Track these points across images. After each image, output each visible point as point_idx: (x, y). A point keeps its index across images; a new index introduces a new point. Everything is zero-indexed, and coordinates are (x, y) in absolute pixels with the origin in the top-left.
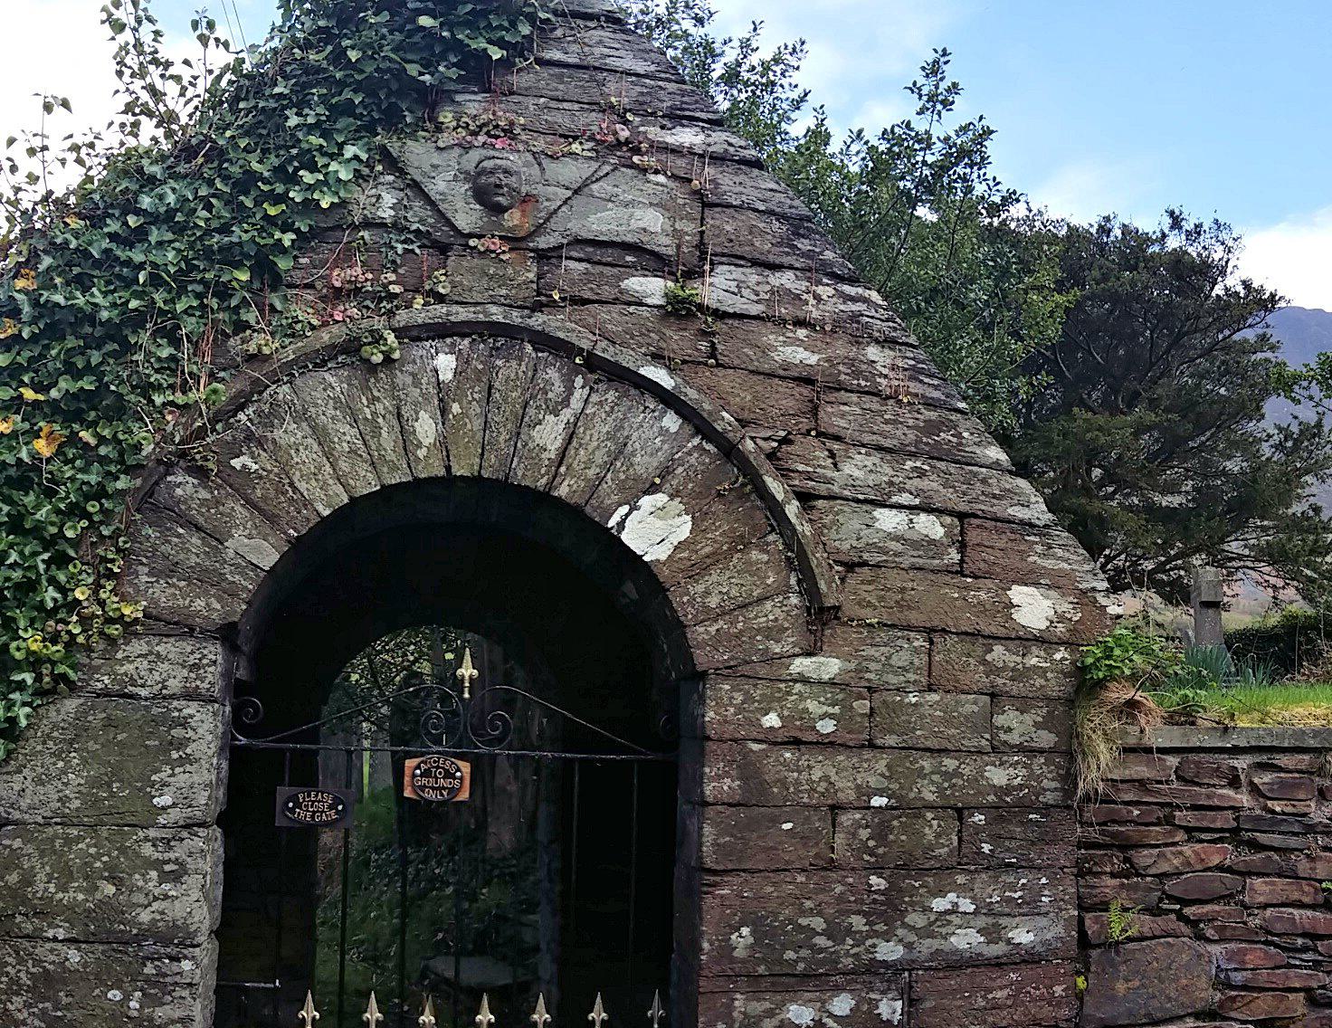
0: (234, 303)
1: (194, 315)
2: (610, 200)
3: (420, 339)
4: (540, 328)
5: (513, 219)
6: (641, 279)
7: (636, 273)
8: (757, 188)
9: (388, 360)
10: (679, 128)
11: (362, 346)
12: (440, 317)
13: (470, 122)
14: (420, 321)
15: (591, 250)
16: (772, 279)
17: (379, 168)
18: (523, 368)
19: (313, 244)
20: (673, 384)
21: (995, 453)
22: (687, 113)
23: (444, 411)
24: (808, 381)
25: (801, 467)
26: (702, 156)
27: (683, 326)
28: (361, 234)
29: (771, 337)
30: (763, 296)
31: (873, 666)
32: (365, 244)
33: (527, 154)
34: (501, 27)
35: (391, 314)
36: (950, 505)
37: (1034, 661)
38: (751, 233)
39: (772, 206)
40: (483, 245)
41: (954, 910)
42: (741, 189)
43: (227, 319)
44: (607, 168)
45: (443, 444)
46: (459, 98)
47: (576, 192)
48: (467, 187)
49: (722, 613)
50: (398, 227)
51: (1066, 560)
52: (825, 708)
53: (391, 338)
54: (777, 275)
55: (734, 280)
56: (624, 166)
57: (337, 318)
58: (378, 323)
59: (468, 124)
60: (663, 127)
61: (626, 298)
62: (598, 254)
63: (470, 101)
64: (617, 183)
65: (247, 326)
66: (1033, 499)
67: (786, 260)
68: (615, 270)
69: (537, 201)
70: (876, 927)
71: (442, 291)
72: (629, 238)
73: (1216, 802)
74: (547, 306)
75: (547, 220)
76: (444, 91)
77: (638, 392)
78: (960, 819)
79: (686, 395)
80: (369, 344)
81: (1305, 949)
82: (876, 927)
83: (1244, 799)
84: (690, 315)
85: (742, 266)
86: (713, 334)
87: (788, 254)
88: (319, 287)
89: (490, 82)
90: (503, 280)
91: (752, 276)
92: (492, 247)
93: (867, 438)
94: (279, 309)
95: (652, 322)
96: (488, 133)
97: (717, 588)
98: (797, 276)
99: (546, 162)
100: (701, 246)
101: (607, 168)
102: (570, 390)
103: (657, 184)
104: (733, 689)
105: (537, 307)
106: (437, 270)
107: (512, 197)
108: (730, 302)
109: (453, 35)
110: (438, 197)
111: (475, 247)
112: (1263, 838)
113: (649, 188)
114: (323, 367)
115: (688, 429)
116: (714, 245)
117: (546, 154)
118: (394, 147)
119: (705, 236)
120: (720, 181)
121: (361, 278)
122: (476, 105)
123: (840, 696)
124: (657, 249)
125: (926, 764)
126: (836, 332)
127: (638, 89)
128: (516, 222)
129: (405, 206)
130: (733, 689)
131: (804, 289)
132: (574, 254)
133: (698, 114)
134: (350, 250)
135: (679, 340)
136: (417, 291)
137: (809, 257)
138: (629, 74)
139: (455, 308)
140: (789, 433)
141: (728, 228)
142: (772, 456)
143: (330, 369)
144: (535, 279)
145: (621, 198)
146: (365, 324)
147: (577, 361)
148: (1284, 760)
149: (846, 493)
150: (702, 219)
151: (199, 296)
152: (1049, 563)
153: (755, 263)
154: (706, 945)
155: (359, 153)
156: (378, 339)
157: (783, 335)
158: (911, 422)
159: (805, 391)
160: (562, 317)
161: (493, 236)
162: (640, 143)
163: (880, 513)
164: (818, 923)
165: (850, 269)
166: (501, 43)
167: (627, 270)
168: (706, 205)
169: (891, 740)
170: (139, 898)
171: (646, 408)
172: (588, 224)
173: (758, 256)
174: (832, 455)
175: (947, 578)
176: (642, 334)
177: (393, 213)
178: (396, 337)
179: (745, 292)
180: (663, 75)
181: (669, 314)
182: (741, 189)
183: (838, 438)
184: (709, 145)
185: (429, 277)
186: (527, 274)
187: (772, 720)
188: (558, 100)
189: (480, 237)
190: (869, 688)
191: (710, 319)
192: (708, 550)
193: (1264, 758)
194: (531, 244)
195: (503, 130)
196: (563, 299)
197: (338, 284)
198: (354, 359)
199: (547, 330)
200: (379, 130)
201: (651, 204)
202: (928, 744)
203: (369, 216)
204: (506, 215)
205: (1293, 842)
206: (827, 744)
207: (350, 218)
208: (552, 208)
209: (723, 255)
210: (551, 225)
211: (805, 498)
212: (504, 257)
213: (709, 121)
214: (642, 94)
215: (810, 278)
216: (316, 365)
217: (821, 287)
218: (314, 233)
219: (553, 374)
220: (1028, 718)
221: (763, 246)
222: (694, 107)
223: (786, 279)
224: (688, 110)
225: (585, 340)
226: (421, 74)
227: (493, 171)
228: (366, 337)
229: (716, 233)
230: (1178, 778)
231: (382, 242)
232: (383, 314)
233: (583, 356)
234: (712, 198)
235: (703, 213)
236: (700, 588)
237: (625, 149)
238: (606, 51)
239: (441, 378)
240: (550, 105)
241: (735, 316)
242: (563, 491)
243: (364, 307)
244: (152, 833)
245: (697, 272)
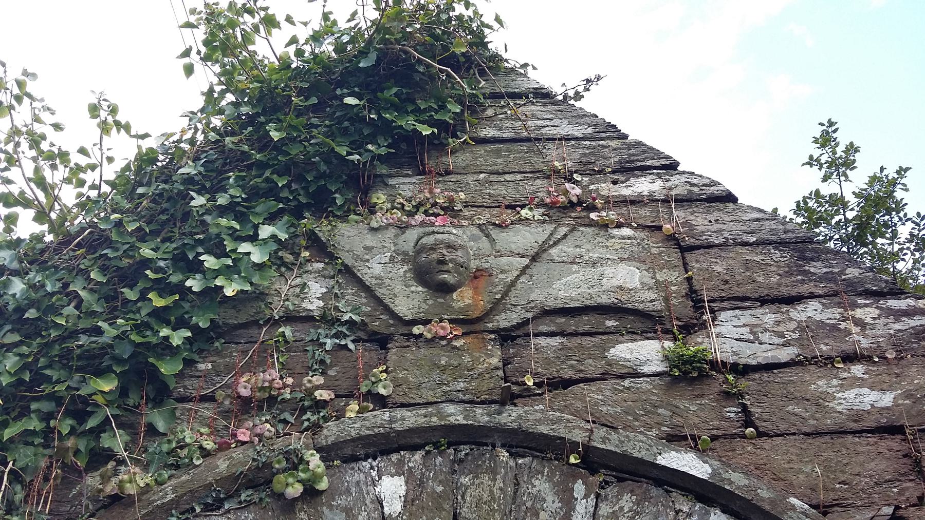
0: (92, 423)
1: (32, 444)
2: (573, 263)
3: (355, 459)
4: (515, 425)
5: (463, 298)
6: (630, 345)
7: (620, 339)
8: (739, 221)
9: (311, 493)
10: (633, 180)
11: (274, 475)
12: (382, 426)
13: (405, 203)
14: (354, 433)
15: (563, 320)
16: (794, 314)
17: (306, 254)
18: (499, 483)
19: (217, 344)
20: (710, 471)
22: (638, 164)
24: (893, 430)
26: (666, 201)
27: (700, 392)
28: (281, 330)
29: (821, 384)
32: (286, 342)
33: (474, 228)
34: (431, 109)
35: (316, 428)
38: (747, 269)
40: (429, 331)
42: (719, 226)
43: (82, 448)
44: (563, 230)
46: (392, 182)
47: (534, 258)
48: (406, 268)
50: (327, 319)
53: (315, 461)
54: (800, 308)
55: (744, 325)
56: (581, 225)
57: (242, 438)
58: (297, 441)
59: (403, 205)
60: (615, 183)
61: (615, 370)
62: (572, 324)
63: (404, 183)
64: (578, 243)
65: (109, 455)
67: (805, 289)
68: (597, 339)
69: (491, 275)
71: (383, 391)
72: (605, 300)
74: (520, 396)
75: (505, 294)
76: (376, 176)
77: (661, 491)
79: (731, 483)
80: (284, 470)
84: (703, 376)
85: (749, 308)
86: (741, 395)
87: (803, 282)
88: (220, 399)
89: (423, 165)
90: (457, 371)
91: (768, 316)
92: (441, 333)
94: (161, 430)
95: (656, 395)
96: (426, 213)
98: (823, 304)
99: (494, 233)
100: (693, 295)
101: (563, 230)
103: (623, 238)
105: (508, 398)
106: (376, 367)
107: (460, 274)
108: (749, 352)
109: (380, 116)
110: (373, 281)
111: (421, 335)
113: (615, 243)
114: (219, 508)
116: (708, 290)
117: (494, 224)
118: (323, 229)
119: (694, 282)
120: (693, 223)
121: (278, 383)
122: (411, 187)
124: (641, 307)
126: (902, 358)
127: (581, 151)
128: (468, 301)
129: (336, 295)
131: (838, 316)
132: (544, 328)
133: (649, 163)
134: (265, 351)
136: (350, 396)
137: (829, 280)
138: (568, 139)
139: (400, 413)
140: (897, 508)
141: (718, 268)
143: (228, 511)
144: (501, 364)
145: (587, 258)
146: (279, 444)
147: (572, 460)
150: (685, 265)
151: (47, 417)
153: (764, 301)
155: (277, 232)
156: (295, 462)
157: (836, 377)
159: (894, 443)
160: (541, 407)
161: (441, 321)
162: (594, 199)
165: (886, 282)
166: (431, 123)
167: (611, 337)
168: (685, 250)
171: (677, 512)
172: (554, 292)
173: (766, 292)
176: (647, 413)
177: (321, 304)
178: (322, 458)
180: (603, 135)
181: (676, 380)
182: (719, 226)
184: (671, 189)
185: (366, 377)
186: (490, 361)
188: (498, 173)
189: (426, 322)
191: (730, 377)
194: (490, 325)
195: (442, 208)
196: (539, 385)
197: (245, 392)
198: (263, 495)
199: (525, 426)
200: (307, 214)
201: (621, 260)
203: (291, 307)
204: (455, 295)
207: (267, 312)
208: (509, 279)
209: (722, 300)
210: (511, 299)
212: (458, 343)
213: (663, 167)
214: (585, 154)
215: (839, 303)
216: (207, 508)
217: (858, 310)
218: (216, 331)
219: (541, 486)
222: (643, 156)
223: (812, 310)
224: (638, 161)
225: (577, 431)
226: (349, 154)
227: (433, 248)
228: (279, 462)
229: (706, 276)
231: (308, 339)
232: (306, 429)
233: (579, 453)
234: (689, 241)
235: (684, 258)
237: (579, 209)
238: (540, 123)
239: (387, 510)
240: (491, 179)
241: (769, 367)
243: (280, 421)
245: (695, 325)
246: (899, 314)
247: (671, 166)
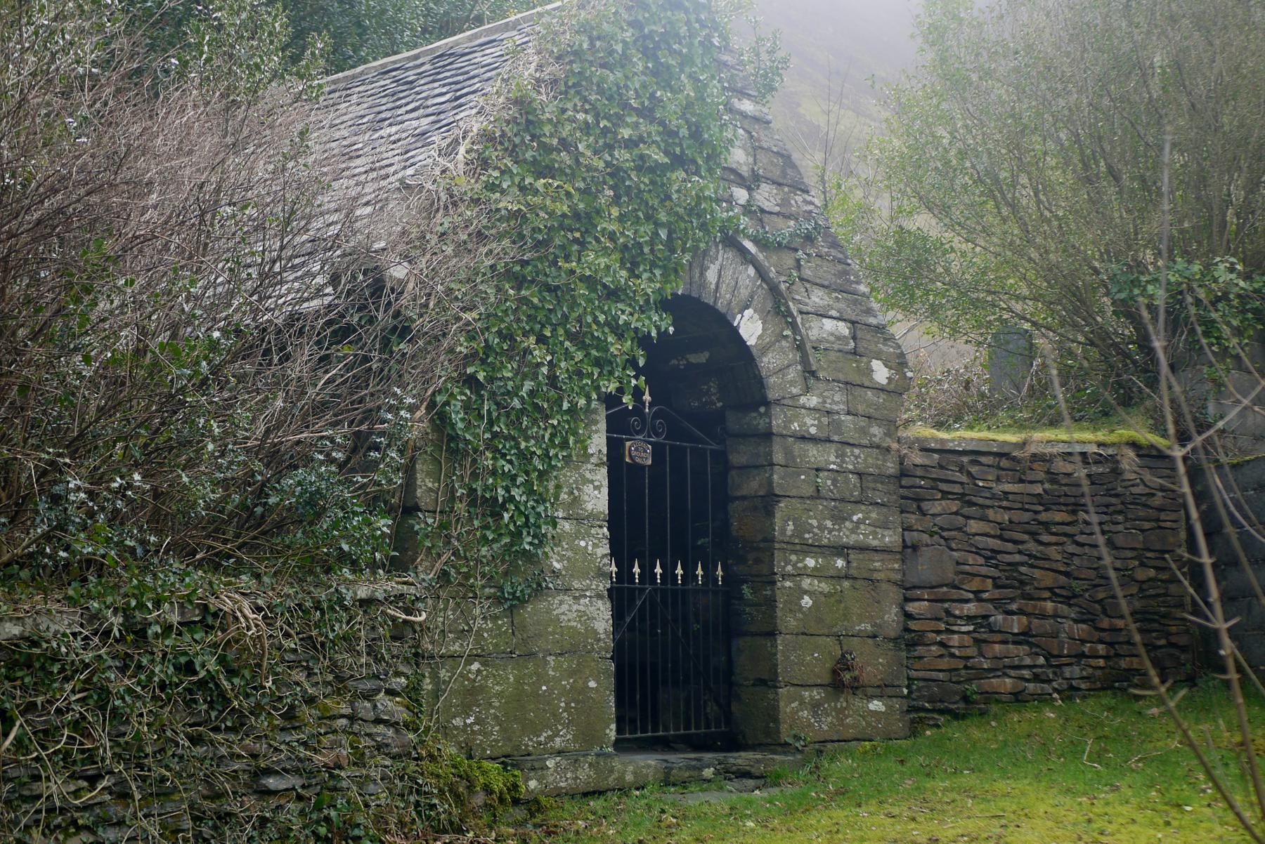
148: (983, 459)
163: (825, 320)
164: (815, 523)
170: (586, 498)
183: (808, 281)
193: (973, 457)
205: (988, 502)
244: (589, 466)
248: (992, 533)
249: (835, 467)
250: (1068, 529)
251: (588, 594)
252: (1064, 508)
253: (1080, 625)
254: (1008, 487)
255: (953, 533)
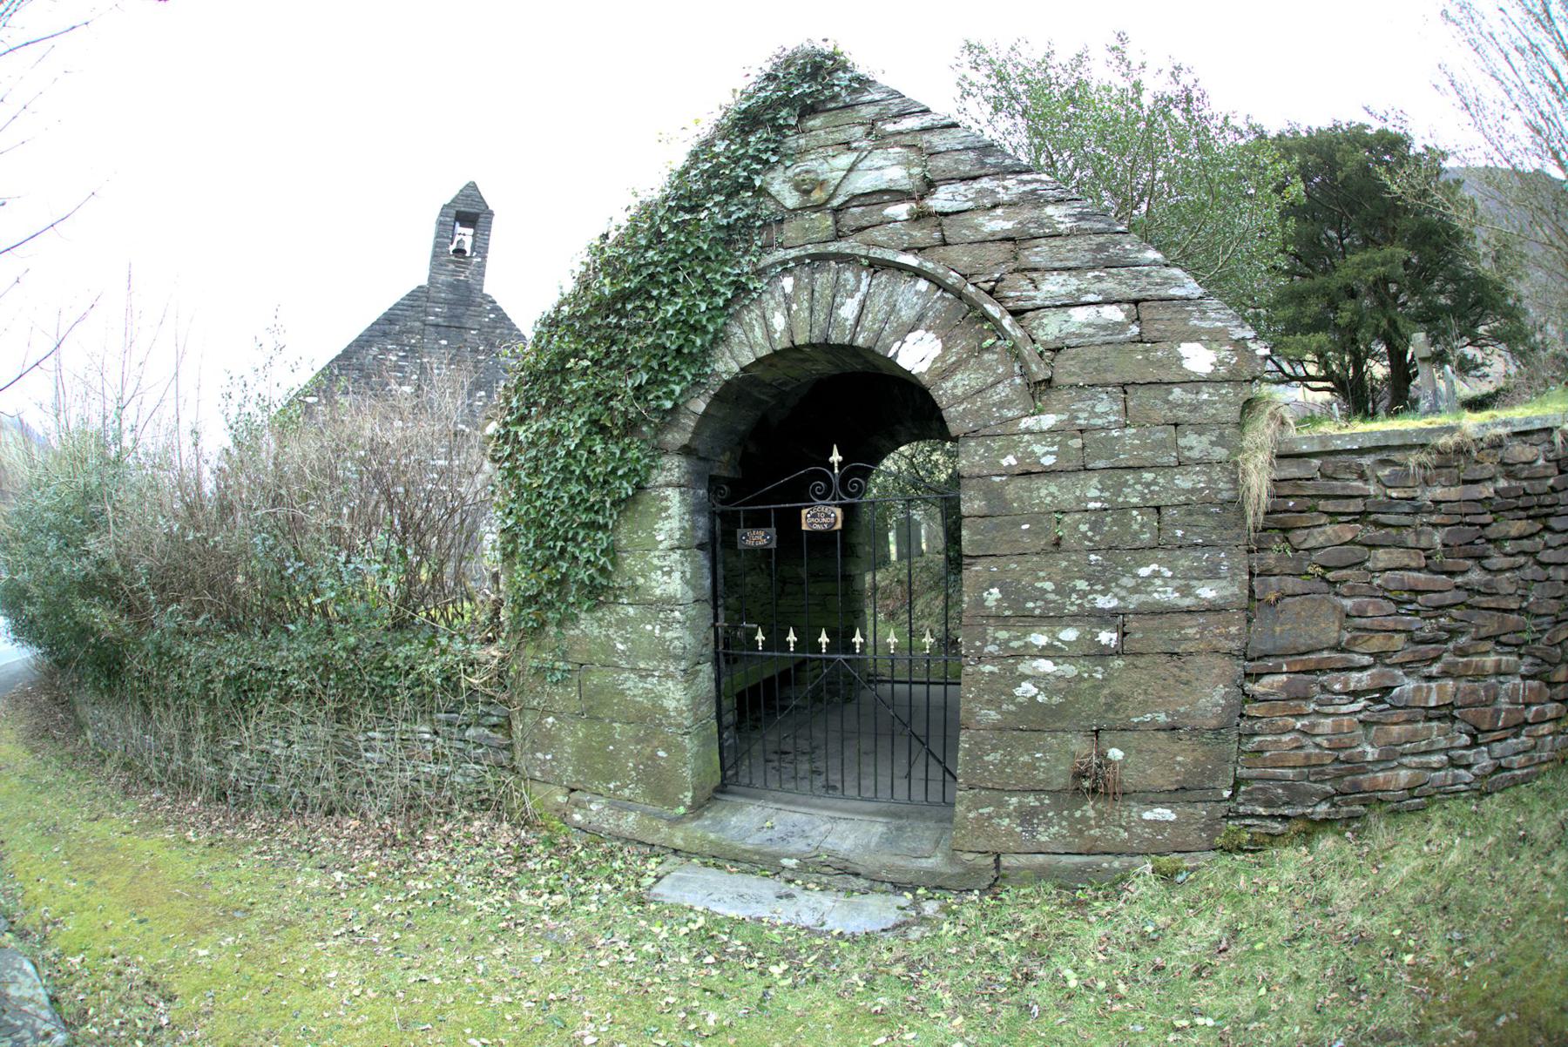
21: (1152, 255)
23: (789, 309)
25: (1012, 294)
29: (980, 219)
30: (970, 196)
31: (1081, 415)
36: (1125, 296)
37: (1205, 396)
39: (967, 145)
41: (1156, 574)
45: (790, 329)
49: (966, 397)
51: (1219, 320)
52: (1046, 449)
66: (1186, 281)
70: (1096, 587)
72: (883, 187)
73: (1349, 492)
78: (1159, 512)
81: (1411, 602)
82: (1096, 587)
83: (1372, 489)
91: (961, 187)
93: (1057, 265)
97: (962, 382)
102: (859, 281)
104: (977, 445)
112: (1383, 518)
115: (934, 287)
123: (1058, 439)
125: (1130, 478)
130: (977, 445)
135: (920, 235)
142: (991, 292)
149: (1047, 303)
152: (1205, 324)
153: (962, 180)
154: (966, 599)
158: (1086, 247)
159: (1009, 245)
164: (1049, 586)
169: (1100, 464)
170: (654, 584)
174: (1033, 281)
175: (1132, 347)
179: (957, 198)
183: (1036, 270)
187: (1010, 460)
190: (1081, 431)
192: (954, 359)
193: (1384, 456)
202: (1131, 463)
205: (1405, 520)
206: (1048, 472)
210: (839, 192)
211: (1017, 313)
220: (1204, 439)
221: (965, 169)
223: (985, 183)
230: (1323, 476)
236: (949, 384)
241: (958, 212)
242: (860, 341)
244: (657, 553)
246: (1025, 183)
247: (926, 111)
248: (1413, 564)
249: (1098, 505)
250: (1526, 544)
251: (656, 674)
252: (1522, 514)
253: (1528, 682)
254: (1438, 492)
255: (1344, 572)
